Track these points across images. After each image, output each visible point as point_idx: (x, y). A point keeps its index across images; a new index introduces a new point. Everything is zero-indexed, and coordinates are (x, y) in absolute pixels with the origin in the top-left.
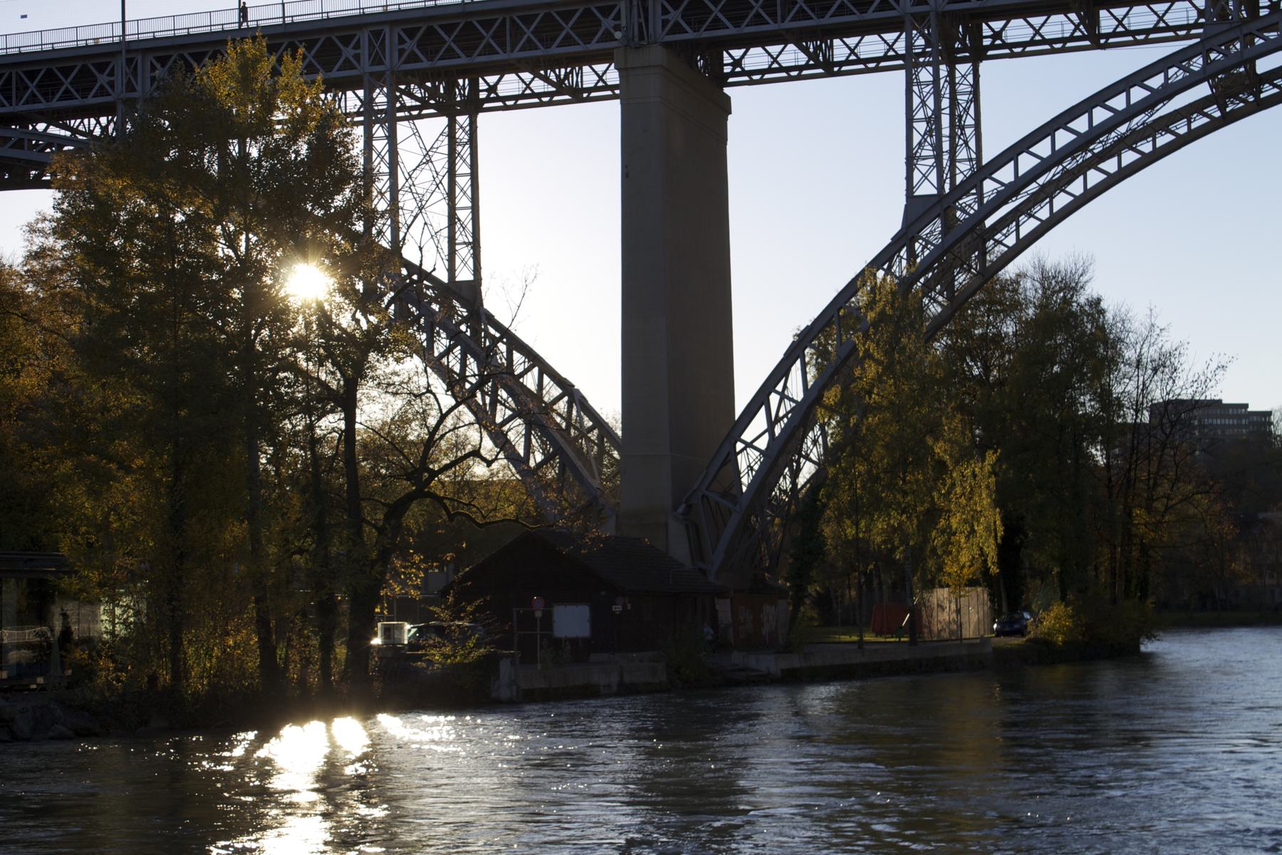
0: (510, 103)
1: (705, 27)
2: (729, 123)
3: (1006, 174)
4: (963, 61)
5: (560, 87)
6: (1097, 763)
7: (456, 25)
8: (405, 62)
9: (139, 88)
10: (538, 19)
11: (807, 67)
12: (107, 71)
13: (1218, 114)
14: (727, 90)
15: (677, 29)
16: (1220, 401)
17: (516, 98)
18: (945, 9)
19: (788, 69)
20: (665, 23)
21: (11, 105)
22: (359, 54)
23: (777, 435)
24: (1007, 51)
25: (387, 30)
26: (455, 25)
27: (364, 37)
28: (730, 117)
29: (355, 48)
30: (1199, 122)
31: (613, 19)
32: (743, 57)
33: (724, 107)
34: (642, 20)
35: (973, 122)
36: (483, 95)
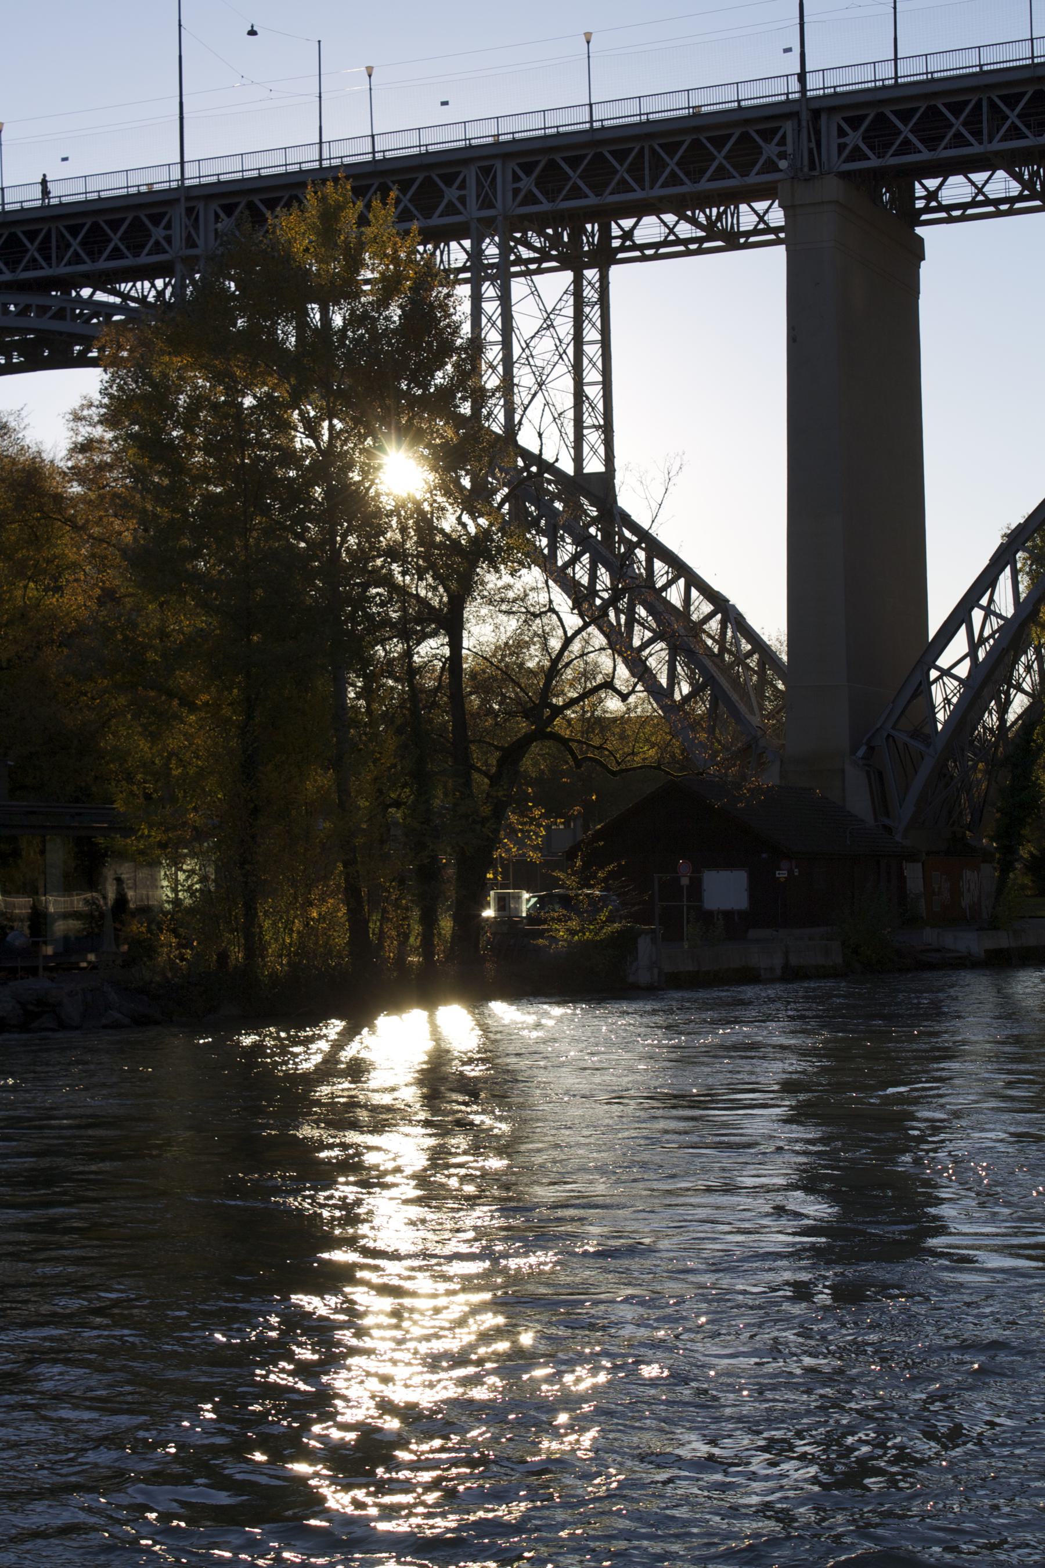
0: (956, 213)
1: (891, 152)
2: (922, 271)
5: (712, 231)
7: (966, 103)
9: (200, 242)
11: (1020, 198)
14: (919, 230)
19: (997, 202)
20: (841, 147)
21: (643, 189)
22: (465, 195)
25: (498, 165)
27: (471, 174)
28: (923, 263)
31: (164, 228)
33: (916, 251)
34: (813, 145)
35: (587, 389)
36: (920, 204)
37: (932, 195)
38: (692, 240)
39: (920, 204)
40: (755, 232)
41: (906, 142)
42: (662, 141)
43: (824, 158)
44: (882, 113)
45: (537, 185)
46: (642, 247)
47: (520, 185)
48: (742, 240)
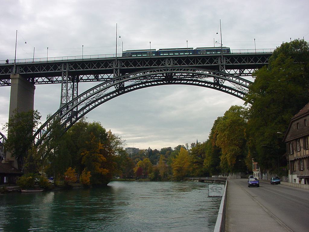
0: (85, 81)
3: (82, 98)
4: (75, 82)
12: (216, 59)
13: (117, 93)
14: (35, 85)
15: (229, 63)
16: (227, 111)
17: (41, 82)
23: (78, 117)
30: (115, 94)
32: (83, 77)
34: (16, 70)
36: (80, 79)
38: (46, 82)
40: (101, 79)
43: (18, 72)
45: (214, 60)
47: (217, 61)
48: (99, 80)
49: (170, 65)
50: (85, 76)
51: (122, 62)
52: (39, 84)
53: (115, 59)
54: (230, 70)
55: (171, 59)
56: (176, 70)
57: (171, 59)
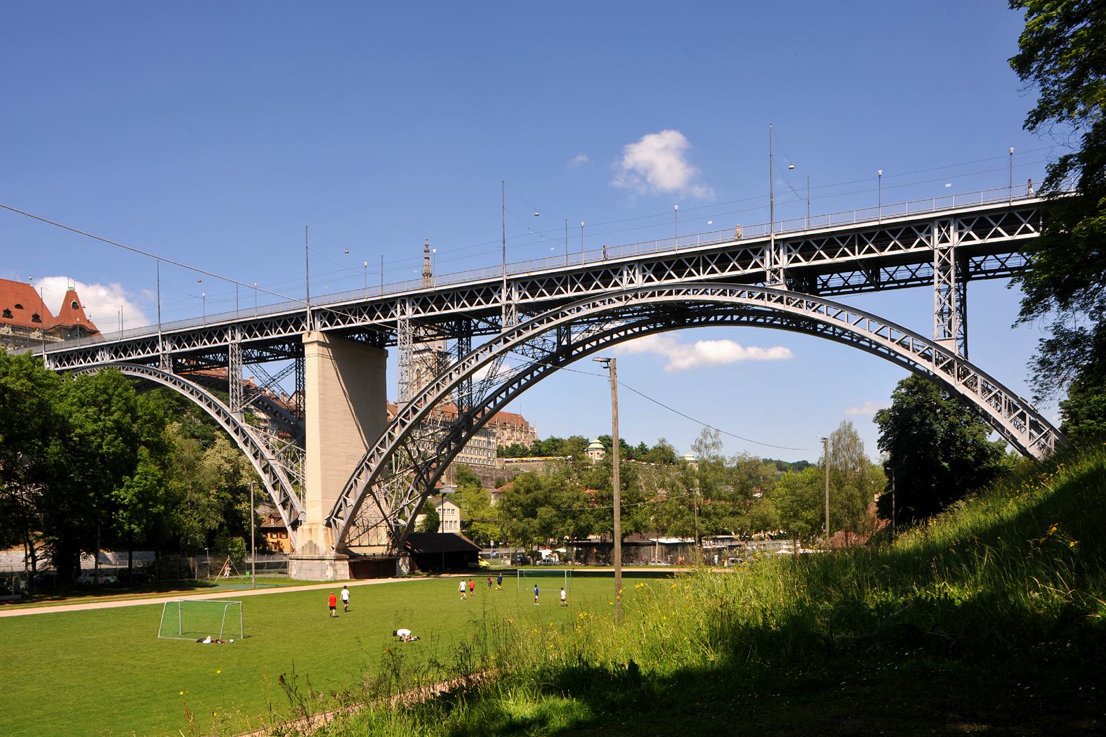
1: (592, 287)
2: (387, 361)
6: (794, 612)
8: (792, 262)
9: (513, 298)
10: (740, 253)
11: (865, 285)
14: (386, 348)
18: (960, 245)
19: (921, 279)
24: (896, 285)
26: (544, 280)
29: (619, 275)
32: (828, 280)
33: (386, 354)
34: (312, 322)
36: (972, 270)
37: (825, 283)
39: (972, 270)
40: (888, 282)
41: (542, 292)
42: (864, 232)
44: (983, 217)
46: (832, 289)
48: (881, 286)
49: (633, 282)
50: (836, 275)
51: (963, 225)
52: (482, 334)
53: (770, 241)
54: (849, 274)
55: (636, 266)
56: (666, 295)
57: (636, 266)
